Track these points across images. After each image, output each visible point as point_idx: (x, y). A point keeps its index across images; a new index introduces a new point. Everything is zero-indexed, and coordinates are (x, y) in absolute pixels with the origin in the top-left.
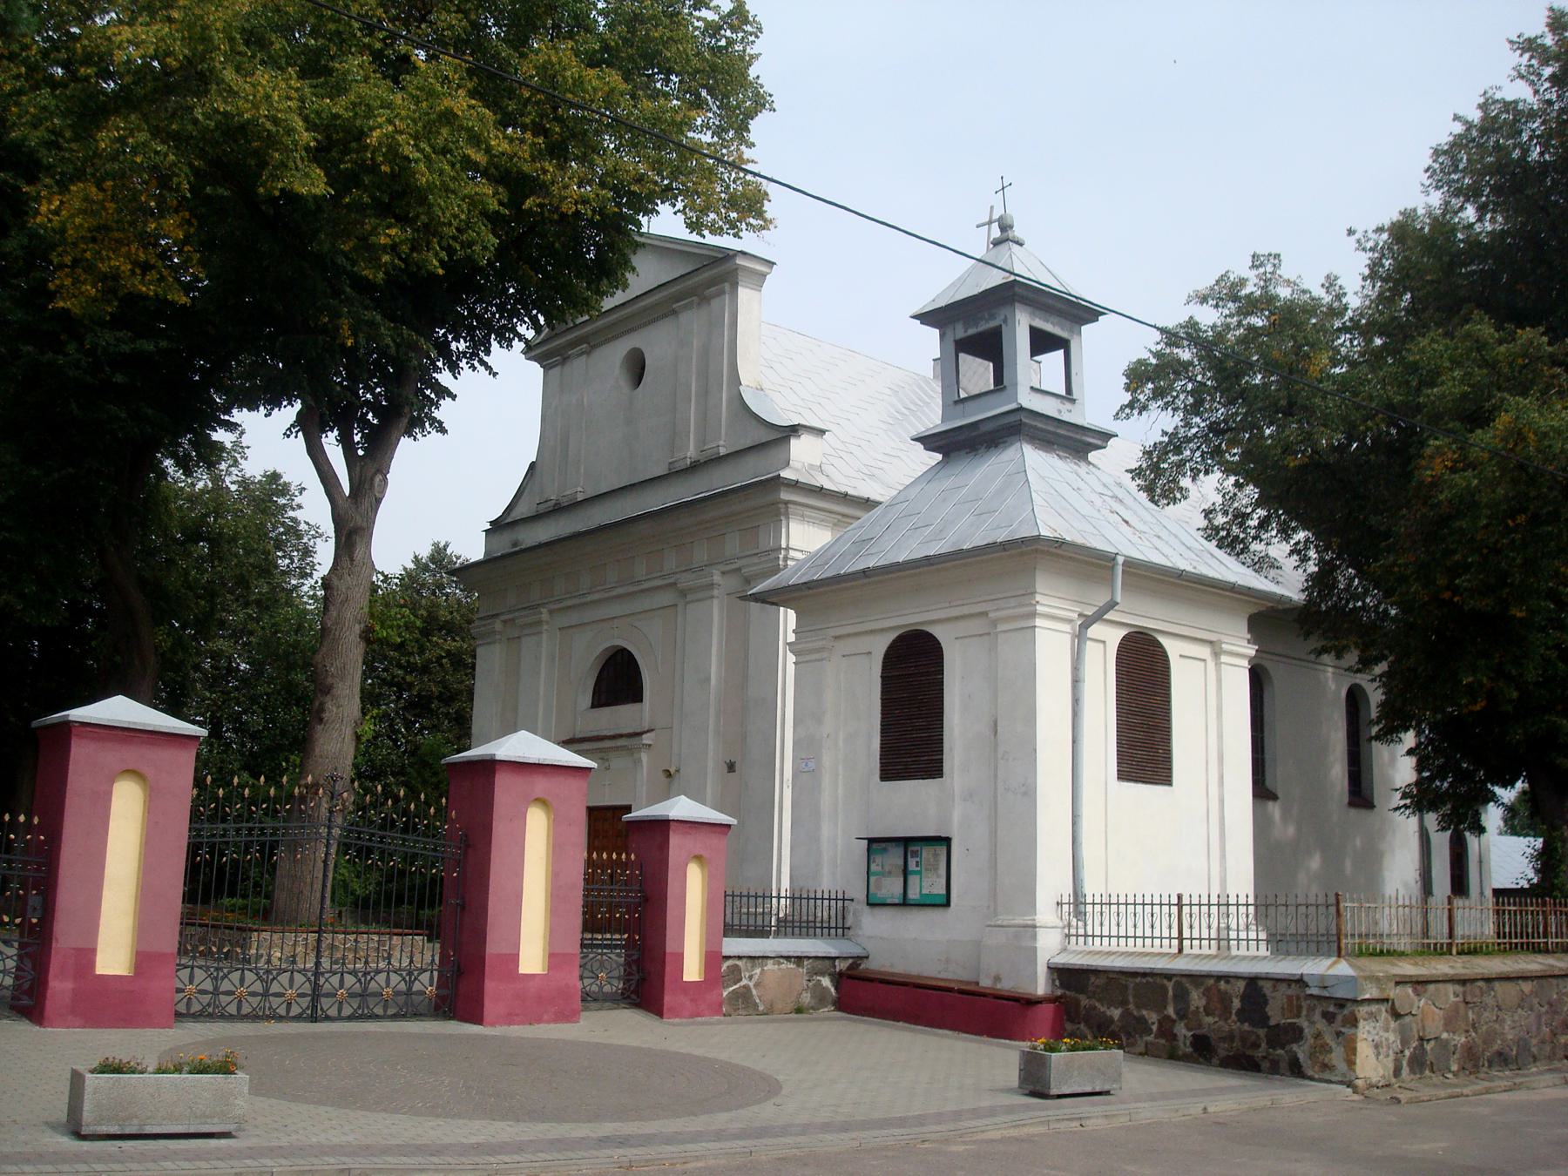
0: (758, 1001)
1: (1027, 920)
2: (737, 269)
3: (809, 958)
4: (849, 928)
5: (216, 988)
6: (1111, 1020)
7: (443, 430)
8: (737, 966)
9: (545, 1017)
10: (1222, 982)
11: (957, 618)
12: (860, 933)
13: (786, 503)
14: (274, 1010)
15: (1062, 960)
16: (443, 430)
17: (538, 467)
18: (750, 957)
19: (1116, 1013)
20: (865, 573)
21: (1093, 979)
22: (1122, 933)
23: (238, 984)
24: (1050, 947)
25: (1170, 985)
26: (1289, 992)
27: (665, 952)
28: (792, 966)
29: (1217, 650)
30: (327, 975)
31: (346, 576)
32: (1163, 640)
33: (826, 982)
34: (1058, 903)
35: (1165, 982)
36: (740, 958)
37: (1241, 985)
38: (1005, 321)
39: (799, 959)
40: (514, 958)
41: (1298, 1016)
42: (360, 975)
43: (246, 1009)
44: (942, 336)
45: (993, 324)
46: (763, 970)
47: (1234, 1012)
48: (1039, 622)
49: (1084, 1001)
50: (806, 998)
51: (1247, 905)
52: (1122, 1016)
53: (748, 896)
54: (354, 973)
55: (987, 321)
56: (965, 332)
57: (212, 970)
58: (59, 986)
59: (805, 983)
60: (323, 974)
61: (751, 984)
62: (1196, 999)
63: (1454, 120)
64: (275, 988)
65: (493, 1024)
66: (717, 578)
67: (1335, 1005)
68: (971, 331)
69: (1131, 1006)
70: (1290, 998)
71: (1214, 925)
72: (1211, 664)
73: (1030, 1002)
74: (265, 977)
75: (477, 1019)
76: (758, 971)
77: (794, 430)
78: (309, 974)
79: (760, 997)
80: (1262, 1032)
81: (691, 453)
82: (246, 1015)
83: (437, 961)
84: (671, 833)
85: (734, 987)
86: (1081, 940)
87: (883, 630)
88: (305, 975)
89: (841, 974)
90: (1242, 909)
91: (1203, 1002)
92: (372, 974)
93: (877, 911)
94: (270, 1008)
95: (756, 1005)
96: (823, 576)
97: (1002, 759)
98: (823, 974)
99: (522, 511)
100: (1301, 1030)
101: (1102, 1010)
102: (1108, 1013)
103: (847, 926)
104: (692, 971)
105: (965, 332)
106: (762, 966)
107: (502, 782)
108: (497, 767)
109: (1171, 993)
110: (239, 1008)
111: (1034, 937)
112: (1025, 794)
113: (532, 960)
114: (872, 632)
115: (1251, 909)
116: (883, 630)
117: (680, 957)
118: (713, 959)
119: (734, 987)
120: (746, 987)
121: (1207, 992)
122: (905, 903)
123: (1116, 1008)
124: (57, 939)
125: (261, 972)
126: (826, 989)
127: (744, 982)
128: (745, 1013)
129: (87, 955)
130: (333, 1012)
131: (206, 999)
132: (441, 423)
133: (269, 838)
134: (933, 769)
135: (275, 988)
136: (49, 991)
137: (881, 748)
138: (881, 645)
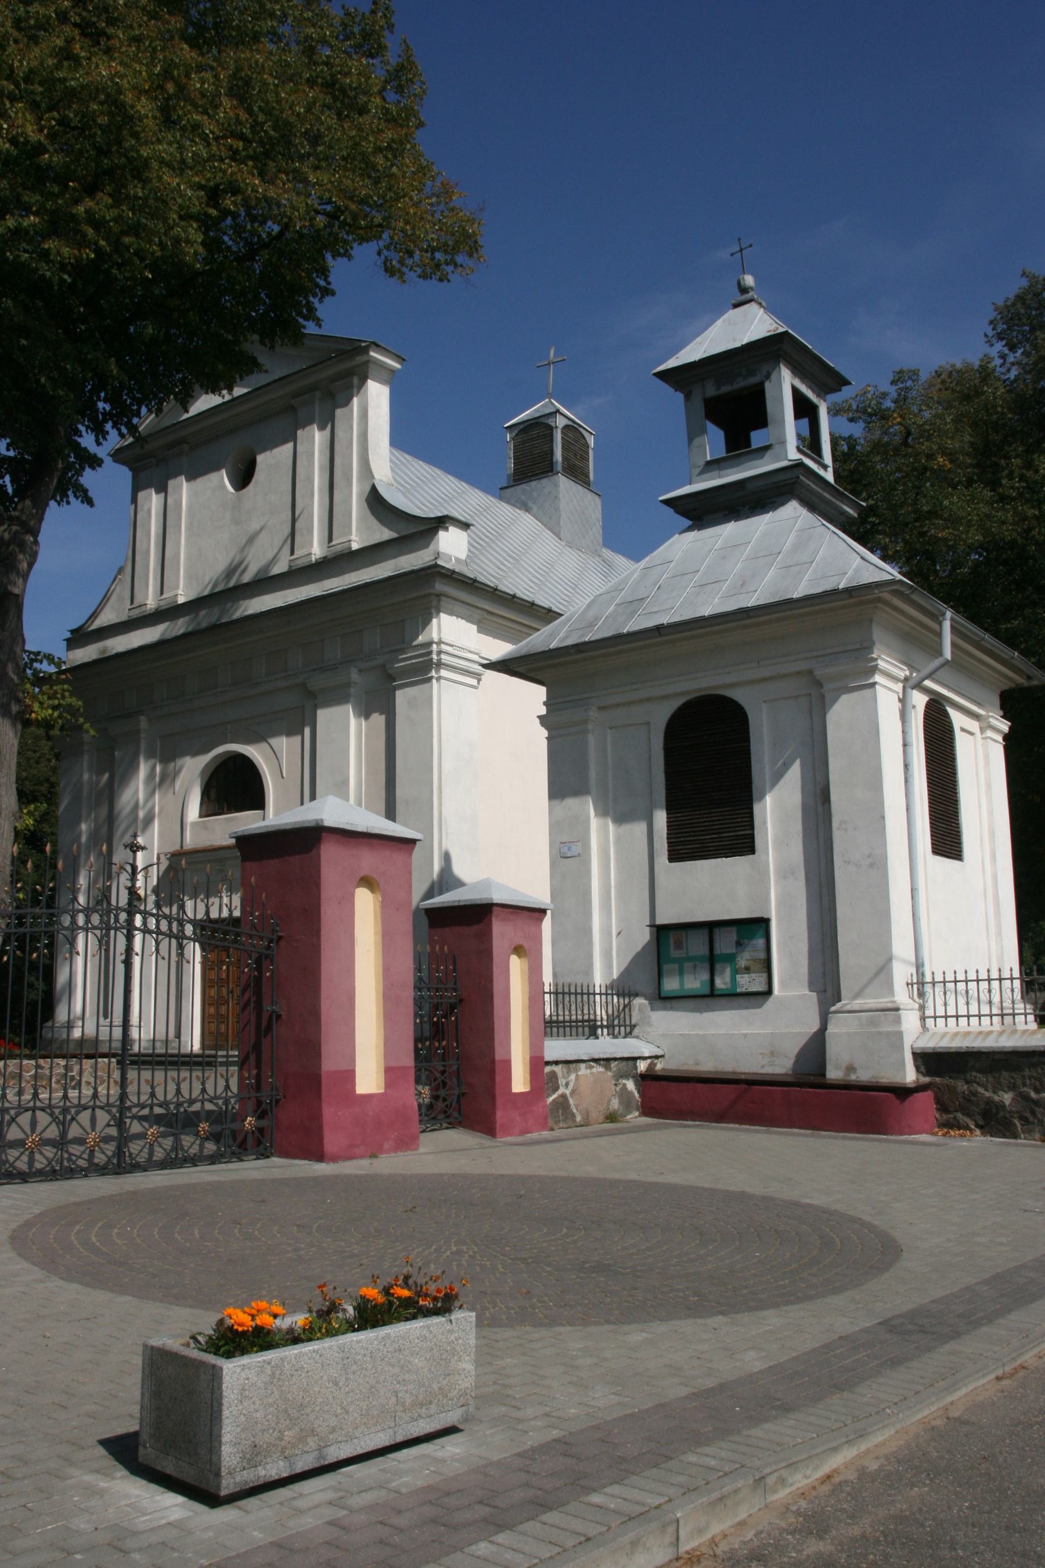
0: (575, 1111)
1: (884, 1002)
2: (369, 362)
3: (615, 1059)
5: (63, 1134)
6: (1001, 1106)
7: (90, 502)
9: (386, 1146)
11: (765, 680)
13: (439, 596)
15: (928, 1043)
16: (90, 502)
18: (567, 1062)
20: (659, 629)
22: (951, 1011)
23: (28, 1130)
27: (493, 1061)
28: (601, 1069)
33: (630, 1085)
34: (908, 984)
36: (557, 1063)
39: (606, 1061)
40: (349, 1076)
43: (40, 1163)
45: (753, 380)
46: (577, 1075)
48: (878, 678)
50: (615, 1104)
51: (1012, 979)
53: (563, 993)
54: (48, 1109)
56: (717, 390)
59: (613, 1087)
60: (129, 1108)
61: (568, 1092)
64: (74, 1131)
65: (334, 1159)
66: (355, 676)
68: (725, 389)
71: (996, 999)
73: (903, 1092)
74: (61, 1117)
75: (320, 1156)
76: (573, 1077)
77: (441, 522)
78: (114, 1110)
79: (576, 1106)
81: (317, 550)
83: (234, 1088)
84: (494, 919)
86: (996, 1019)
87: (666, 697)
88: (109, 1112)
90: (1007, 984)
94: (69, 1160)
95: (573, 1116)
96: (593, 639)
97: (838, 829)
98: (627, 1077)
102: (996, 1098)
104: (520, 1082)
105: (718, 389)
106: (577, 1070)
107: (329, 853)
108: (324, 835)
111: (898, 1021)
114: (649, 700)
115: (1017, 984)
116: (666, 697)
117: (507, 1063)
118: (537, 1064)
120: (563, 1096)
125: (57, 1111)
126: (631, 1093)
128: (565, 1125)
132: (85, 491)
135: (74, 1131)
137: (668, 826)
138: (662, 714)
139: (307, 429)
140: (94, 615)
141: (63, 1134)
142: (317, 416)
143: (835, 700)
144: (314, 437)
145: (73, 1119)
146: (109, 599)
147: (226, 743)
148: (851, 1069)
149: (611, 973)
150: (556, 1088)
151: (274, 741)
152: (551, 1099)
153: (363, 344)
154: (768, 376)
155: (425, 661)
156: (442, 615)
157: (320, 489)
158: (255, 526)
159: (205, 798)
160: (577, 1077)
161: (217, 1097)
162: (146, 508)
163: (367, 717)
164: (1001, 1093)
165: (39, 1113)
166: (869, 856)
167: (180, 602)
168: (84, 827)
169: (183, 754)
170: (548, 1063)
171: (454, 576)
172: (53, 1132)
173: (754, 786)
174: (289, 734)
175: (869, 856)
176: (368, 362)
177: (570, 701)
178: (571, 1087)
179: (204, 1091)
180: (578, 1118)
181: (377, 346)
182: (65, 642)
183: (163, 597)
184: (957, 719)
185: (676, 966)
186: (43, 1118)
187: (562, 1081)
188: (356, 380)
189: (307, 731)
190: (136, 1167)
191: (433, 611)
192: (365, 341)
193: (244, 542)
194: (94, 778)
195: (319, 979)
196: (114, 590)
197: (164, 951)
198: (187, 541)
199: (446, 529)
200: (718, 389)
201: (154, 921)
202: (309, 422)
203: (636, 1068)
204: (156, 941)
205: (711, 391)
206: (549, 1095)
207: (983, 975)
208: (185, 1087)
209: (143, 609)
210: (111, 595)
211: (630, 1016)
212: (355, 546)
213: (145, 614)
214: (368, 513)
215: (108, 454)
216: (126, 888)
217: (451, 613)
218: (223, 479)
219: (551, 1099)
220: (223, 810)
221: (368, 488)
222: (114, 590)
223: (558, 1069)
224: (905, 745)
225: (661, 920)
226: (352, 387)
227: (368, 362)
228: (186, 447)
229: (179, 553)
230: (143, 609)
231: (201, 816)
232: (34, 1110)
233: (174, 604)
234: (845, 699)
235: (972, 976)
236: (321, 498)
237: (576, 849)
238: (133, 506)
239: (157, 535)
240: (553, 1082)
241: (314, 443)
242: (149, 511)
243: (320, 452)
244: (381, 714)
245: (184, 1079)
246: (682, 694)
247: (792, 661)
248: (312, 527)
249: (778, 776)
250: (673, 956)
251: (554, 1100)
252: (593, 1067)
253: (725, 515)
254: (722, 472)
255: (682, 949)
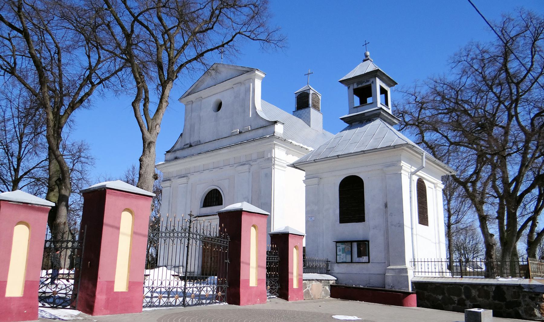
3: (323, 280)
4: (329, 270)
5: (152, 295)
8: (305, 283)
10: (485, 287)
12: (333, 272)
13: (275, 144)
14: (171, 303)
17: (183, 134)
19: (440, 297)
24: (412, 276)
25: (463, 288)
26: (514, 290)
29: (436, 186)
30: (188, 289)
31: (148, 157)
32: (424, 181)
35: (461, 287)
36: (306, 280)
37: (494, 288)
38: (373, 82)
39: (320, 281)
41: (519, 297)
42: (199, 288)
44: (349, 88)
47: (491, 297)
49: (426, 293)
52: (442, 298)
55: (366, 83)
56: (357, 86)
57: (151, 288)
58: (100, 297)
60: (187, 288)
62: (474, 293)
67: (535, 294)
68: (360, 86)
69: (446, 295)
70: (515, 292)
72: (434, 189)
80: (503, 303)
82: (178, 305)
85: (305, 290)
89: (331, 286)
91: (477, 293)
92: (202, 288)
93: (340, 264)
95: (311, 296)
98: (326, 285)
99: (178, 146)
100: (520, 303)
101: (434, 296)
102: (437, 297)
103: (329, 270)
105: (358, 86)
106: (312, 283)
109: (463, 290)
110: (159, 302)
112: (399, 226)
113: (253, 283)
118: (300, 281)
119: (305, 290)
120: (308, 290)
121: (479, 290)
122: (352, 262)
123: (440, 295)
124: (99, 277)
127: (307, 288)
129: (111, 284)
130: (190, 303)
131: (148, 300)
134: (361, 219)
136: (96, 299)
152: (304, 291)
164: (438, 296)
170: (304, 280)
175: (399, 223)
184: (427, 184)
200: (358, 86)
205: (356, 86)
219: (304, 291)
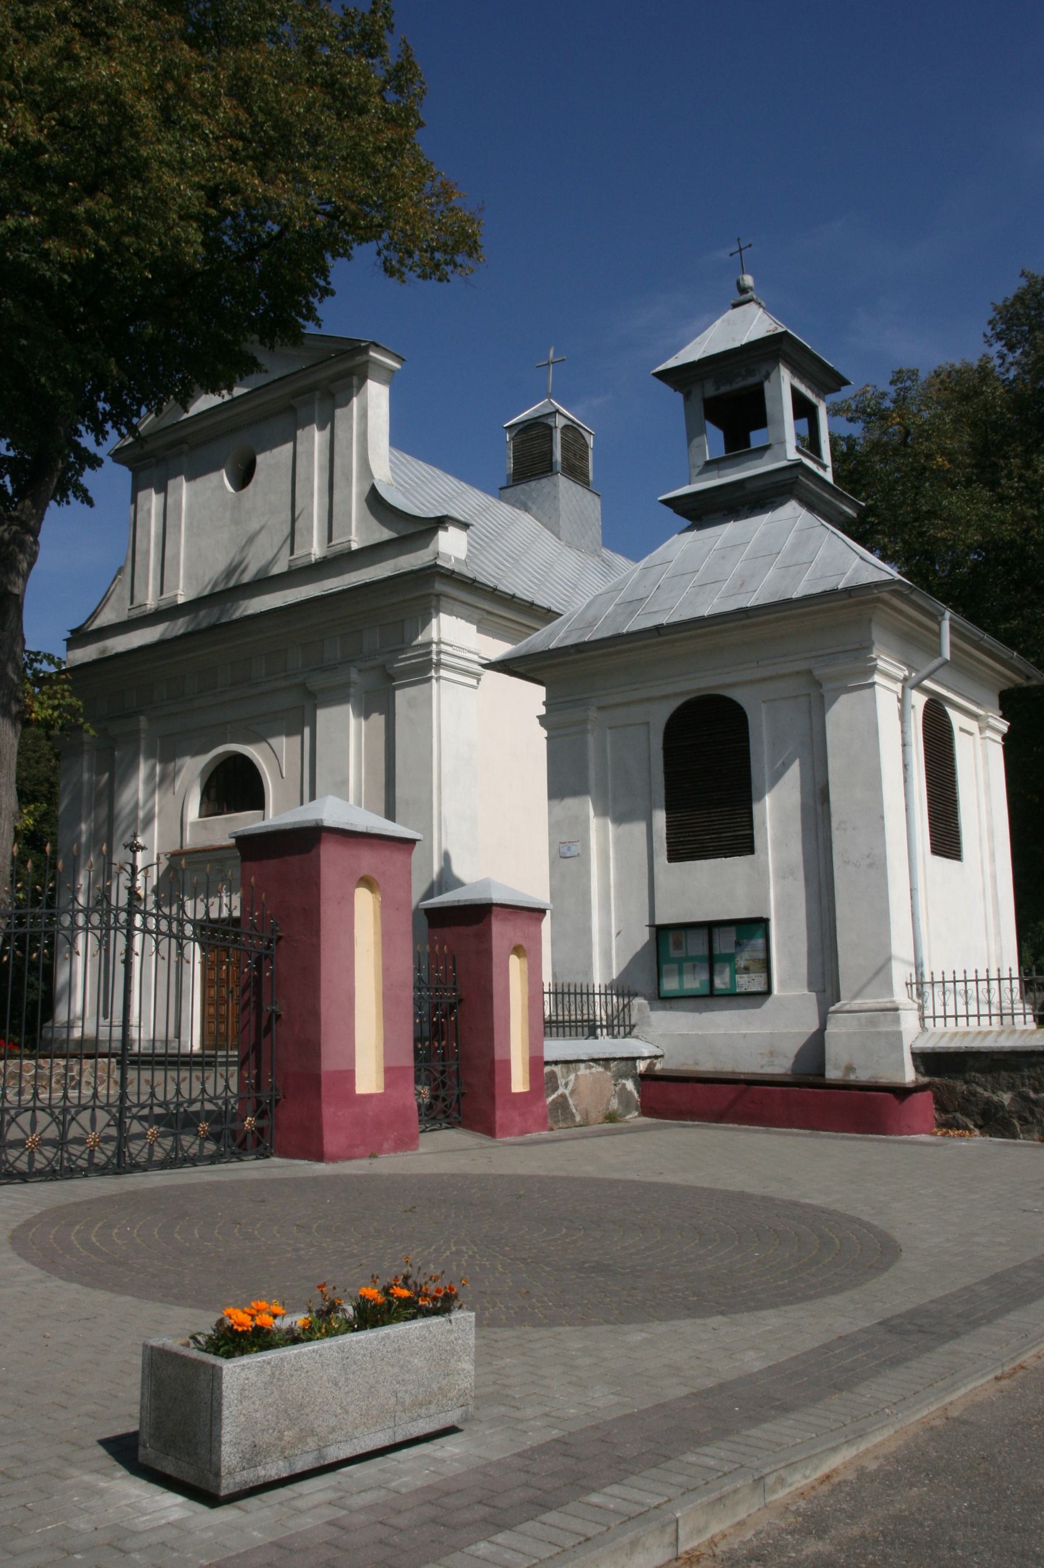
0: (574, 1111)
1: (883, 1002)
2: (368, 362)
3: (614, 1059)
5: (63, 1134)
6: (1000, 1106)
7: (90, 502)
9: (386, 1146)
11: (764, 680)
13: (439, 596)
15: (927, 1043)
16: (90, 502)
18: (567, 1062)
20: (658, 629)
21: (206, 1043)
22: (950, 1011)
23: (28, 1130)
27: (493, 1061)
28: (600, 1069)
33: (630, 1085)
34: (907, 984)
36: (556, 1063)
39: (606, 1061)
40: (348, 1076)
45: (752, 380)
46: (577, 1075)
48: (877, 678)
50: (615, 1104)
51: (1011, 979)
53: (563, 993)
54: (48, 1109)
56: (716, 390)
59: (612, 1087)
60: (129, 1108)
61: (567, 1092)
63: (1021, 276)
64: (74, 1131)
65: (334, 1159)
66: (354, 676)
68: (724, 389)
71: (995, 999)
73: (902, 1092)
74: (61, 1117)
75: (319, 1156)
76: (572, 1077)
77: (441, 522)
78: (114, 1110)
79: (576, 1106)
81: (316, 550)
83: (234, 1088)
84: (493, 919)
86: (995, 1019)
87: (666, 697)
88: (109, 1112)
90: (1006, 984)
95: (573, 1116)
96: (592, 639)
97: (838, 829)
98: (626, 1077)
102: (995, 1098)
104: (519, 1082)
105: (717, 389)
106: (576, 1070)
107: (329, 853)
108: (324, 835)
111: (897, 1021)
114: (649, 700)
115: (1016, 984)
116: (666, 697)
117: (507, 1063)
118: (537, 1064)
120: (563, 1096)
125: (57, 1111)
126: (630, 1093)
128: (565, 1125)
132: (85, 491)
133: (29, 929)
135: (74, 1131)
137: (667, 826)
138: (661, 714)
139: (307, 429)
140: (94, 615)
141: (63, 1134)
142: (316, 416)
143: (834, 700)
144: (313, 437)
145: (73, 1119)
146: (108, 599)
147: (226, 743)
148: (850, 1069)
149: (611, 973)
150: (556, 1088)
151: (273, 741)
152: (550, 1099)
153: (363, 344)
154: (767, 376)
155: (424, 661)
156: (441, 615)
157: (320, 489)
158: (255, 526)
159: (205, 798)
160: (577, 1077)
161: (216, 1097)
162: (146, 508)
163: (367, 717)
164: (1000, 1093)
165: (39, 1113)
166: (868, 856)
167: (180, 602)
168: (84, 827)
169: (183, 754)
170: (547, 1063)
171: (454, 576)
172: (53, 1132)
173: (753, 786)
174: (289, 734)
175: (868, 856)
176: (367, 362)
177: (569, 701)
178: (570, 1087)
179: (203, 1091)
180: (578, 1118)
181: (377, 346)
182: (65, 642)
183: (163, 597)
185: (675, 966)
186: (43, 1118)
187: (561, 1081)
188: (355, 380)
189: (307, 731)
190: (136, 1167)
191: (433, 611)
192: (365, 341)
193: (244, 542)
194: (94, 778)
195: (319, 979)
196: (114, 590)
197: (164, 951)
198: (187, 541)
199: (446, 529)
200: (717, 389)
201: (154, 921)
202: (309, 422)
203: (635, 1068)
204: (156, 941)
205: (710, 391)
206: (549, 1095)
207: (982, 975)
208: (184, 1087)
209: (143, 609)
210: (111, 595)
211: (630, 1016)
212: (355, 546)
213: (145, 614)
214: (368, 513)
215: (108, 454)
216: (126, 888)
217: (451, 613)
218: (223, 479)
219: (550, 1099)
220: (223, 810)
221: (368, 488)
222: (114, 590)
223: (557, 1069)
224: (904, 745)
225: (661, 920)
226: (352, 387)
227: (367, 362)
228: (185, 447)
229: (179, 553)
230: (143, 609)
231: (200, 816)
232: (34, 1110)
233: (174, 604)
234: (844, 699)
235: (971, 976)
236: (320, 498)
237: (575, 849)
238: (133, 506)
239: (157, 535)
240: (552, 1082)
241: (313, 443)
242: (149, 511)
243: (320, 452)
244: (380, 714)
245: (184, 1079)
246: (682, 694)
247: (792, 661)
248: (312, 527)
249: (777, 776)
250: (672, 956)
251: (553, 1100)
252: (593, 1067)
253: (725, 515)
254: (721, 472)
255: (681, 949)
